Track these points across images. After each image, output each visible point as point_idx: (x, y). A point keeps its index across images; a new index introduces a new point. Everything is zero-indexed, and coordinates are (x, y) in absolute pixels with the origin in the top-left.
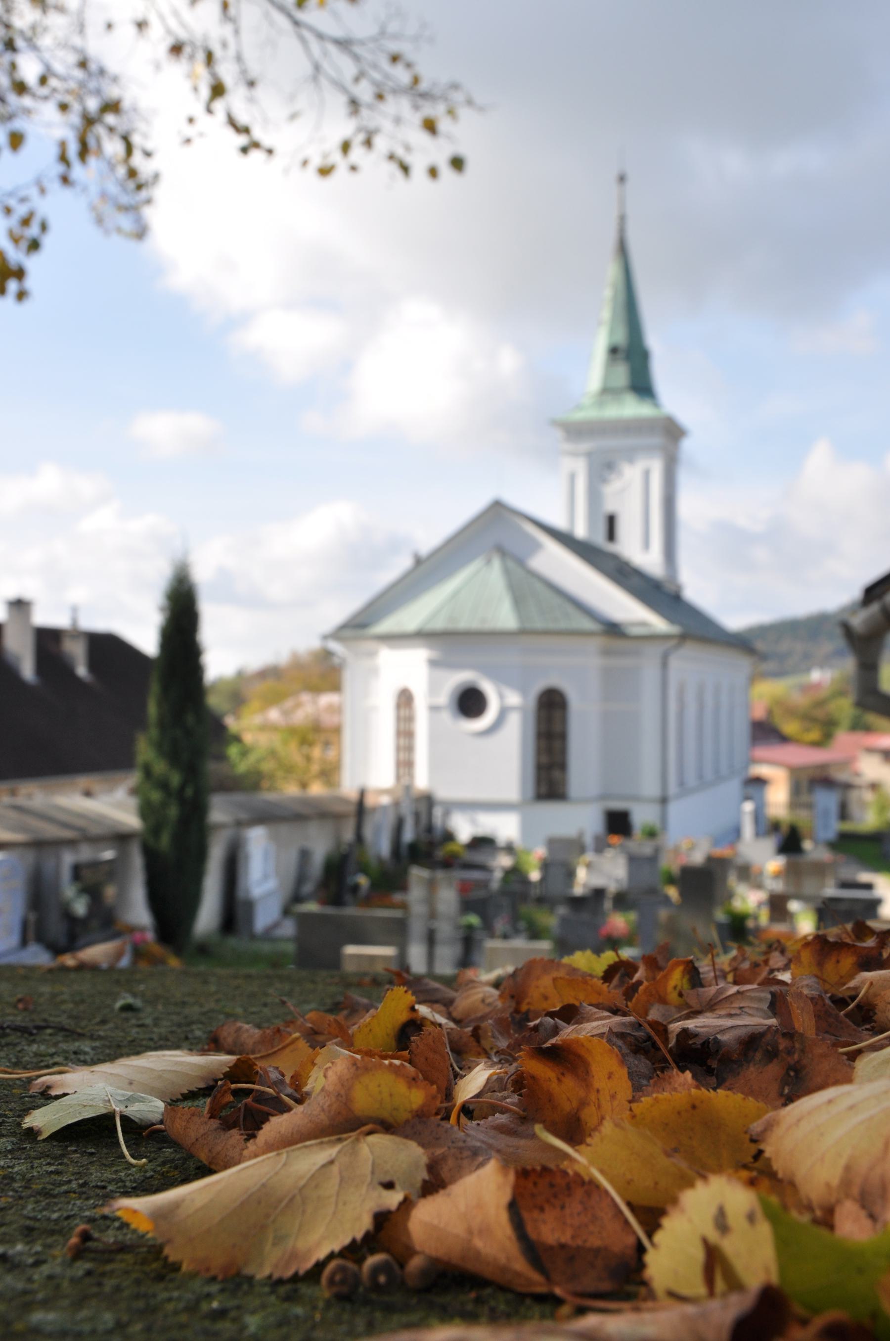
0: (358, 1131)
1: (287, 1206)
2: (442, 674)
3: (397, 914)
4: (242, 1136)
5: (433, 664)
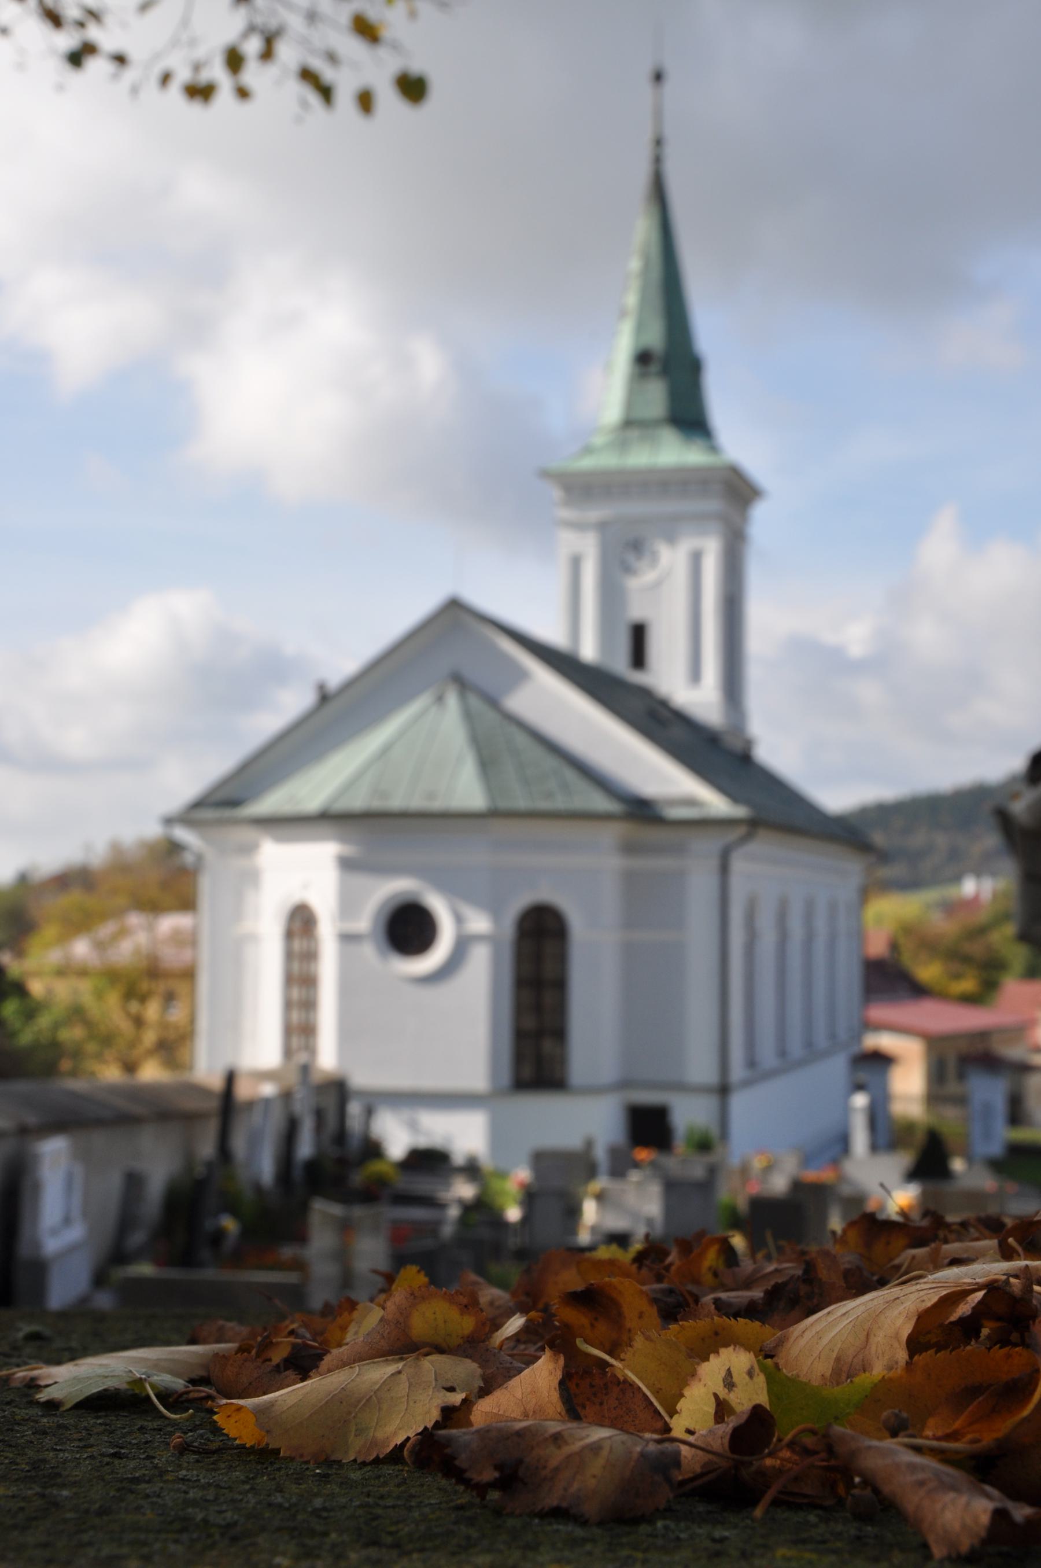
0: (417, 1353)
1: (364, 1405)
2: (361, 880)
3: (291, 1278)
4: (297, 1376)
5: (346, 864)
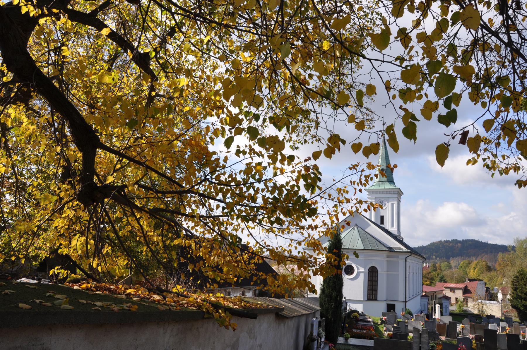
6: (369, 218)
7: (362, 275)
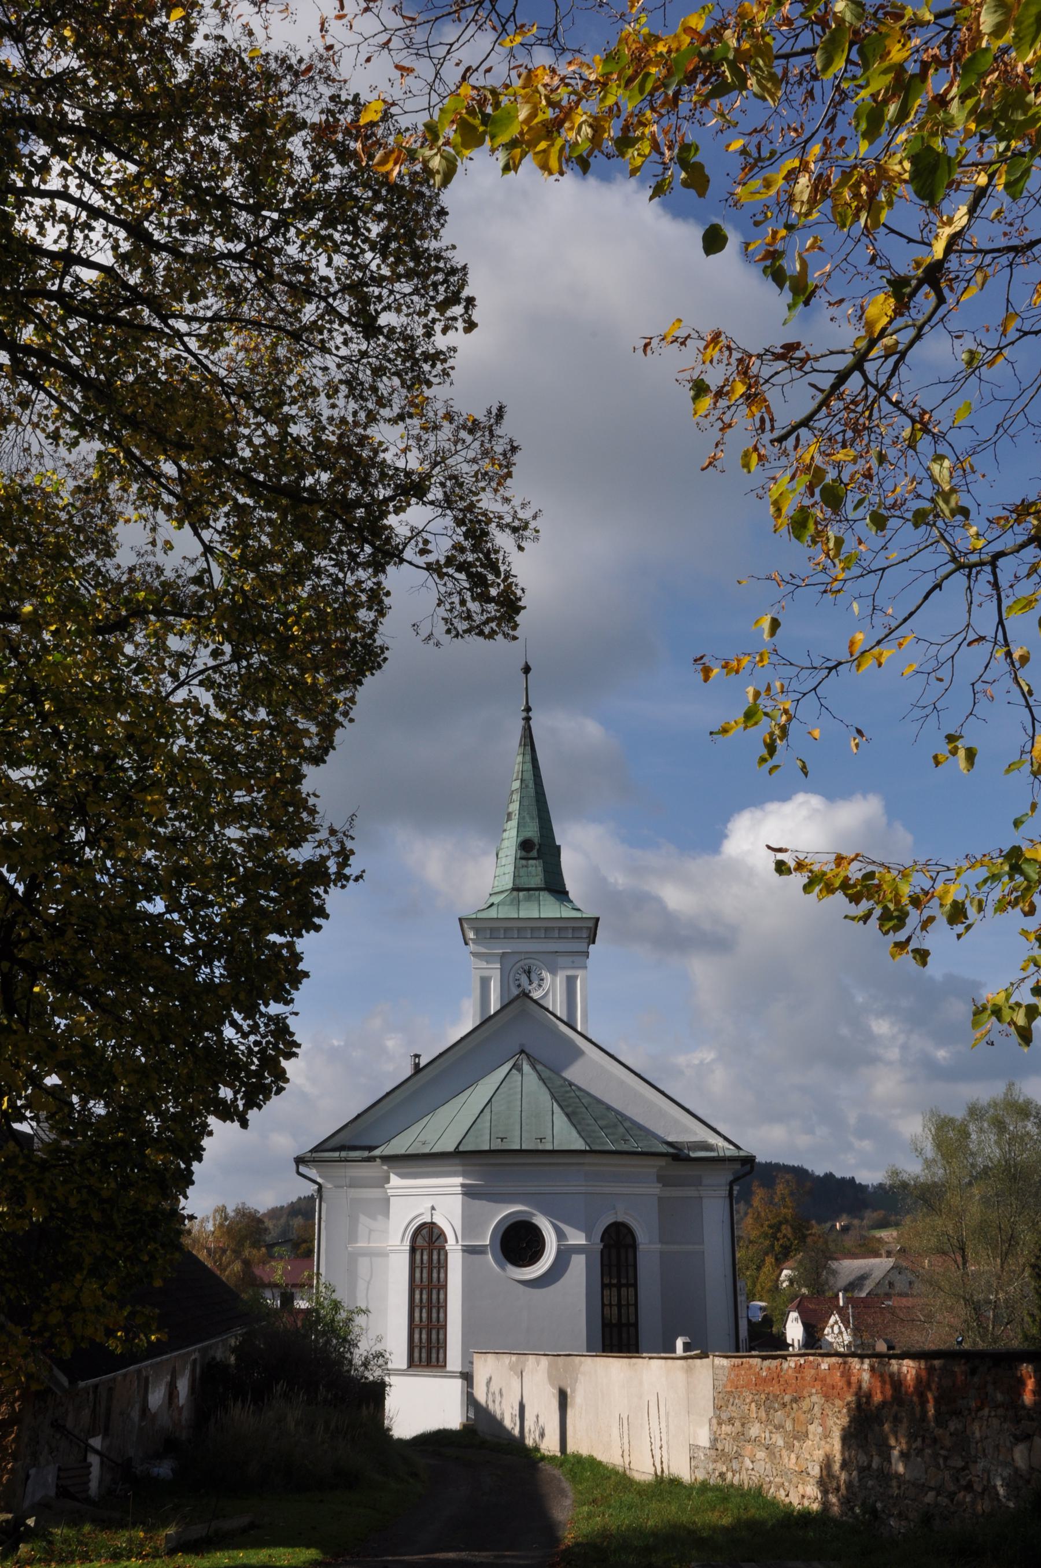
5: (469, 1192)
6: (565, 1018)
7: (578, 1264)
